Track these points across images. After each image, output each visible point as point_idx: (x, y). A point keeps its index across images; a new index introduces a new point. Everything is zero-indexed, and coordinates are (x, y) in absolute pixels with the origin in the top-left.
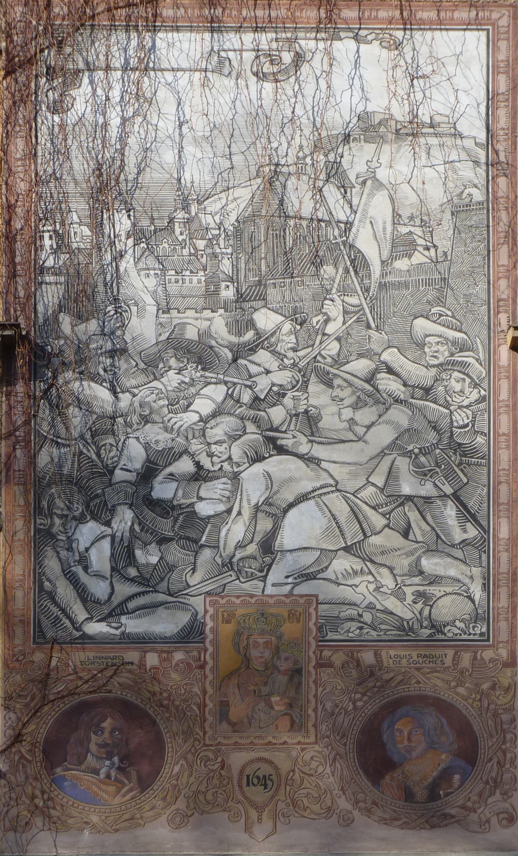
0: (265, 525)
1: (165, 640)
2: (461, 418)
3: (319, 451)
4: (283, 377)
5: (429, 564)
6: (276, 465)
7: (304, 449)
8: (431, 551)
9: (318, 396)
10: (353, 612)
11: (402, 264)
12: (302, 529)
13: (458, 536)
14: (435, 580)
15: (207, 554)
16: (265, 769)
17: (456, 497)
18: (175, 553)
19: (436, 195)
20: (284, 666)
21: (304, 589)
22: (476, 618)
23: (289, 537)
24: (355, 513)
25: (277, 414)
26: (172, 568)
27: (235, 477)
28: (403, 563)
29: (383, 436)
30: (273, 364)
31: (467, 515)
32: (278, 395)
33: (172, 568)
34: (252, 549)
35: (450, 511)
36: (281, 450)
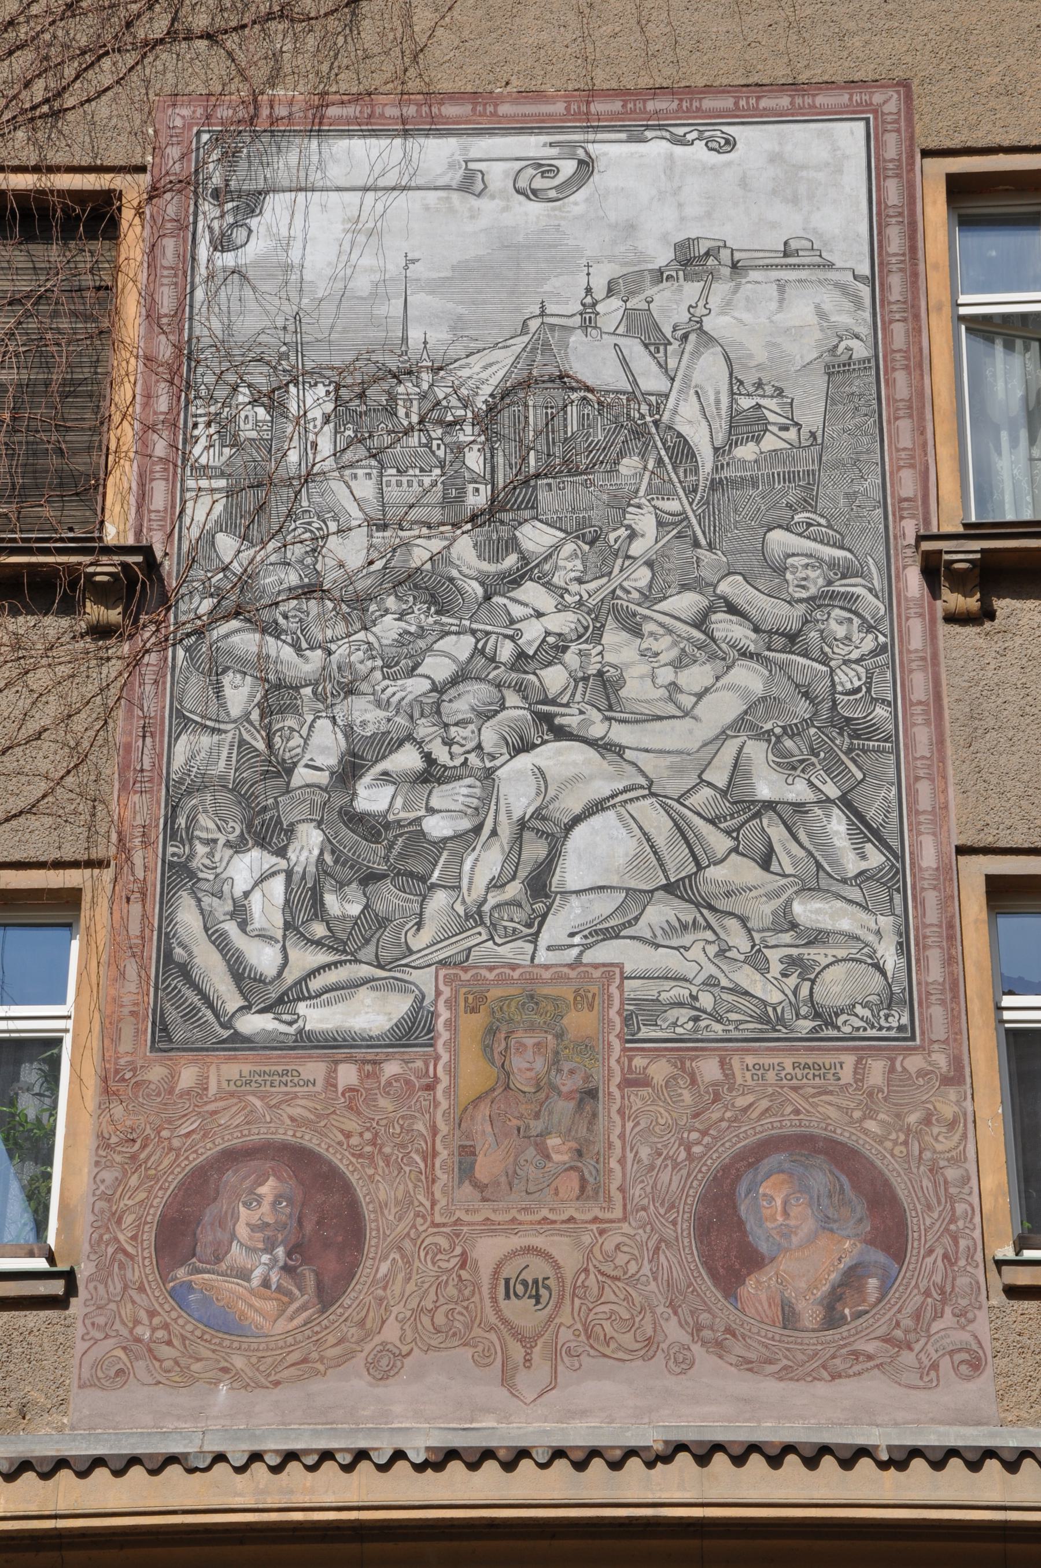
0: (535, 850)
1: (369, 1042)
2: (847, 678)
3: (620, 734)
4: (563, 623)
5: (808, 911)
6: (554, 756)
7: (597, 730)
8: (808, 889)
9: (618, 647)
10: (680, 992)
11: (746, 452)
12: (598, 854)
13: (852, 865)
14: (817, 938)
15: (440, 899)
16: (538, 1269)
17: (845, 802)
18: (390, 897)
19: (806, 350)
20: (568, 1084)
21: (605, 953)
22: (890, 1002)
23: (573, 871)
24: (680, 829)
25: (554, 678)
26: (383, 922)
27: (488, 775)
28: (762, 911)
29: (722, 709)
30: (545, 601)
31: (866, 830)
32: (555, 649)
33: (383, 922)
34: (514, 890)
35: (838, 825)
36: (561, 733)
